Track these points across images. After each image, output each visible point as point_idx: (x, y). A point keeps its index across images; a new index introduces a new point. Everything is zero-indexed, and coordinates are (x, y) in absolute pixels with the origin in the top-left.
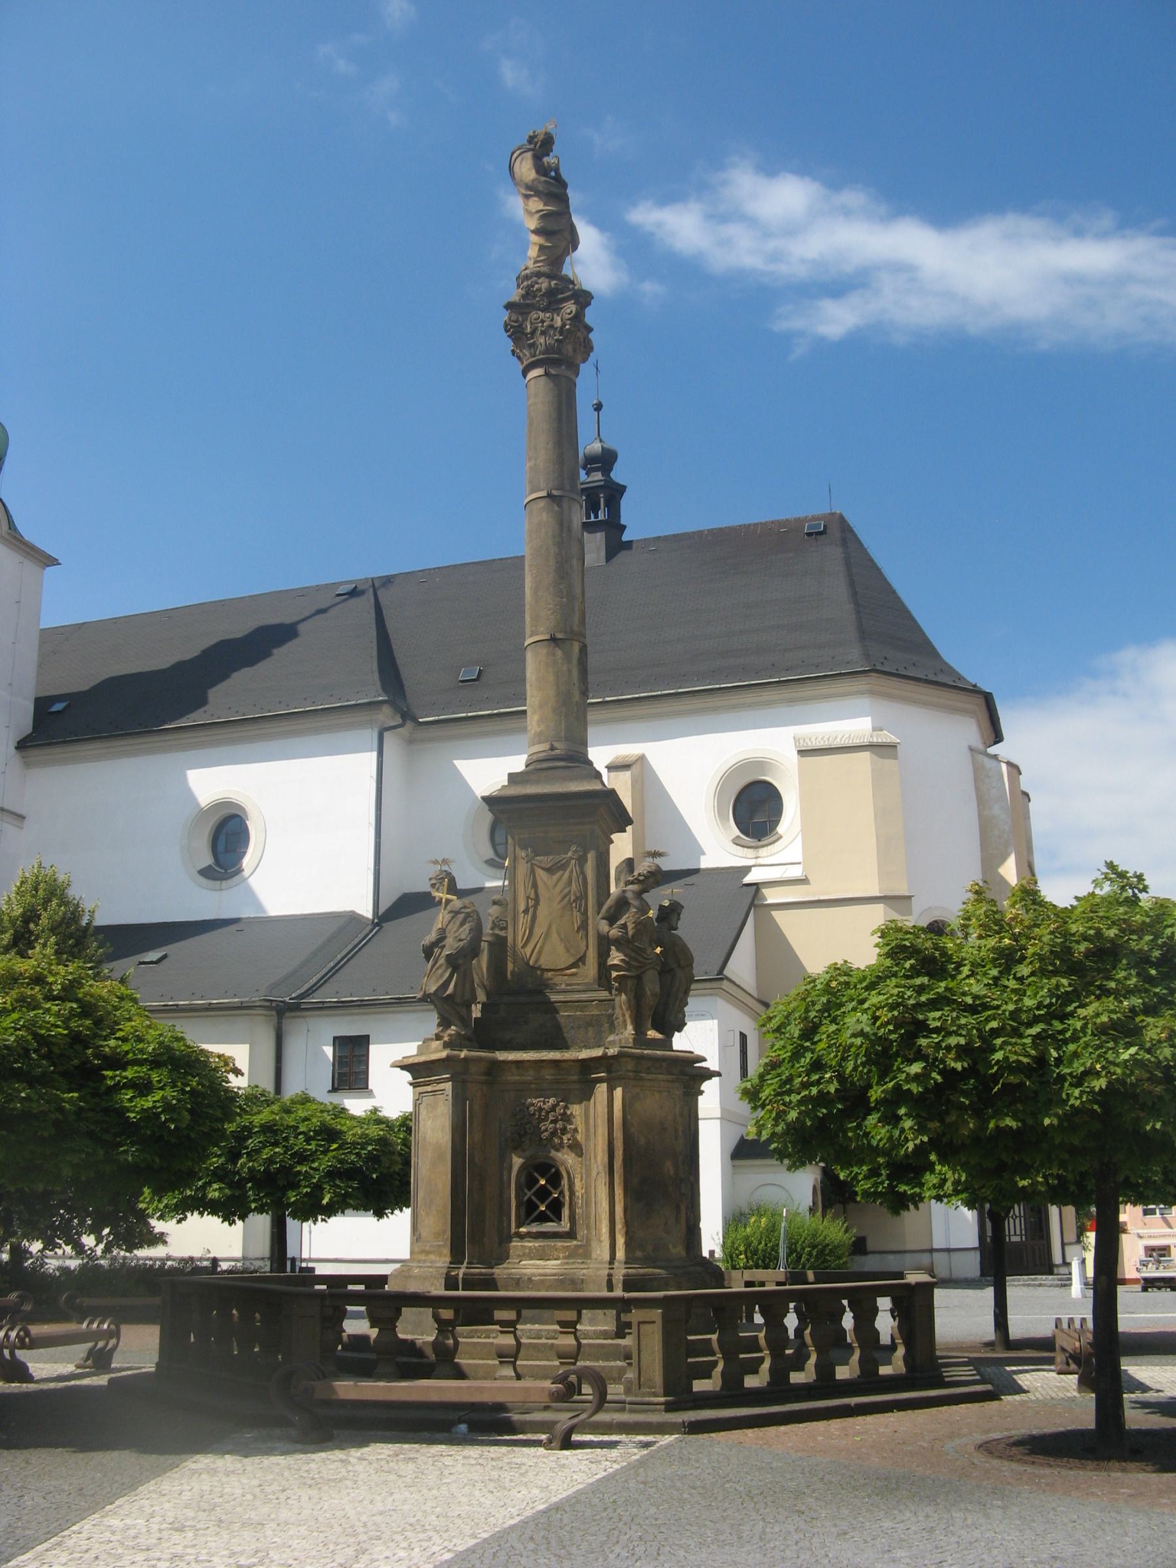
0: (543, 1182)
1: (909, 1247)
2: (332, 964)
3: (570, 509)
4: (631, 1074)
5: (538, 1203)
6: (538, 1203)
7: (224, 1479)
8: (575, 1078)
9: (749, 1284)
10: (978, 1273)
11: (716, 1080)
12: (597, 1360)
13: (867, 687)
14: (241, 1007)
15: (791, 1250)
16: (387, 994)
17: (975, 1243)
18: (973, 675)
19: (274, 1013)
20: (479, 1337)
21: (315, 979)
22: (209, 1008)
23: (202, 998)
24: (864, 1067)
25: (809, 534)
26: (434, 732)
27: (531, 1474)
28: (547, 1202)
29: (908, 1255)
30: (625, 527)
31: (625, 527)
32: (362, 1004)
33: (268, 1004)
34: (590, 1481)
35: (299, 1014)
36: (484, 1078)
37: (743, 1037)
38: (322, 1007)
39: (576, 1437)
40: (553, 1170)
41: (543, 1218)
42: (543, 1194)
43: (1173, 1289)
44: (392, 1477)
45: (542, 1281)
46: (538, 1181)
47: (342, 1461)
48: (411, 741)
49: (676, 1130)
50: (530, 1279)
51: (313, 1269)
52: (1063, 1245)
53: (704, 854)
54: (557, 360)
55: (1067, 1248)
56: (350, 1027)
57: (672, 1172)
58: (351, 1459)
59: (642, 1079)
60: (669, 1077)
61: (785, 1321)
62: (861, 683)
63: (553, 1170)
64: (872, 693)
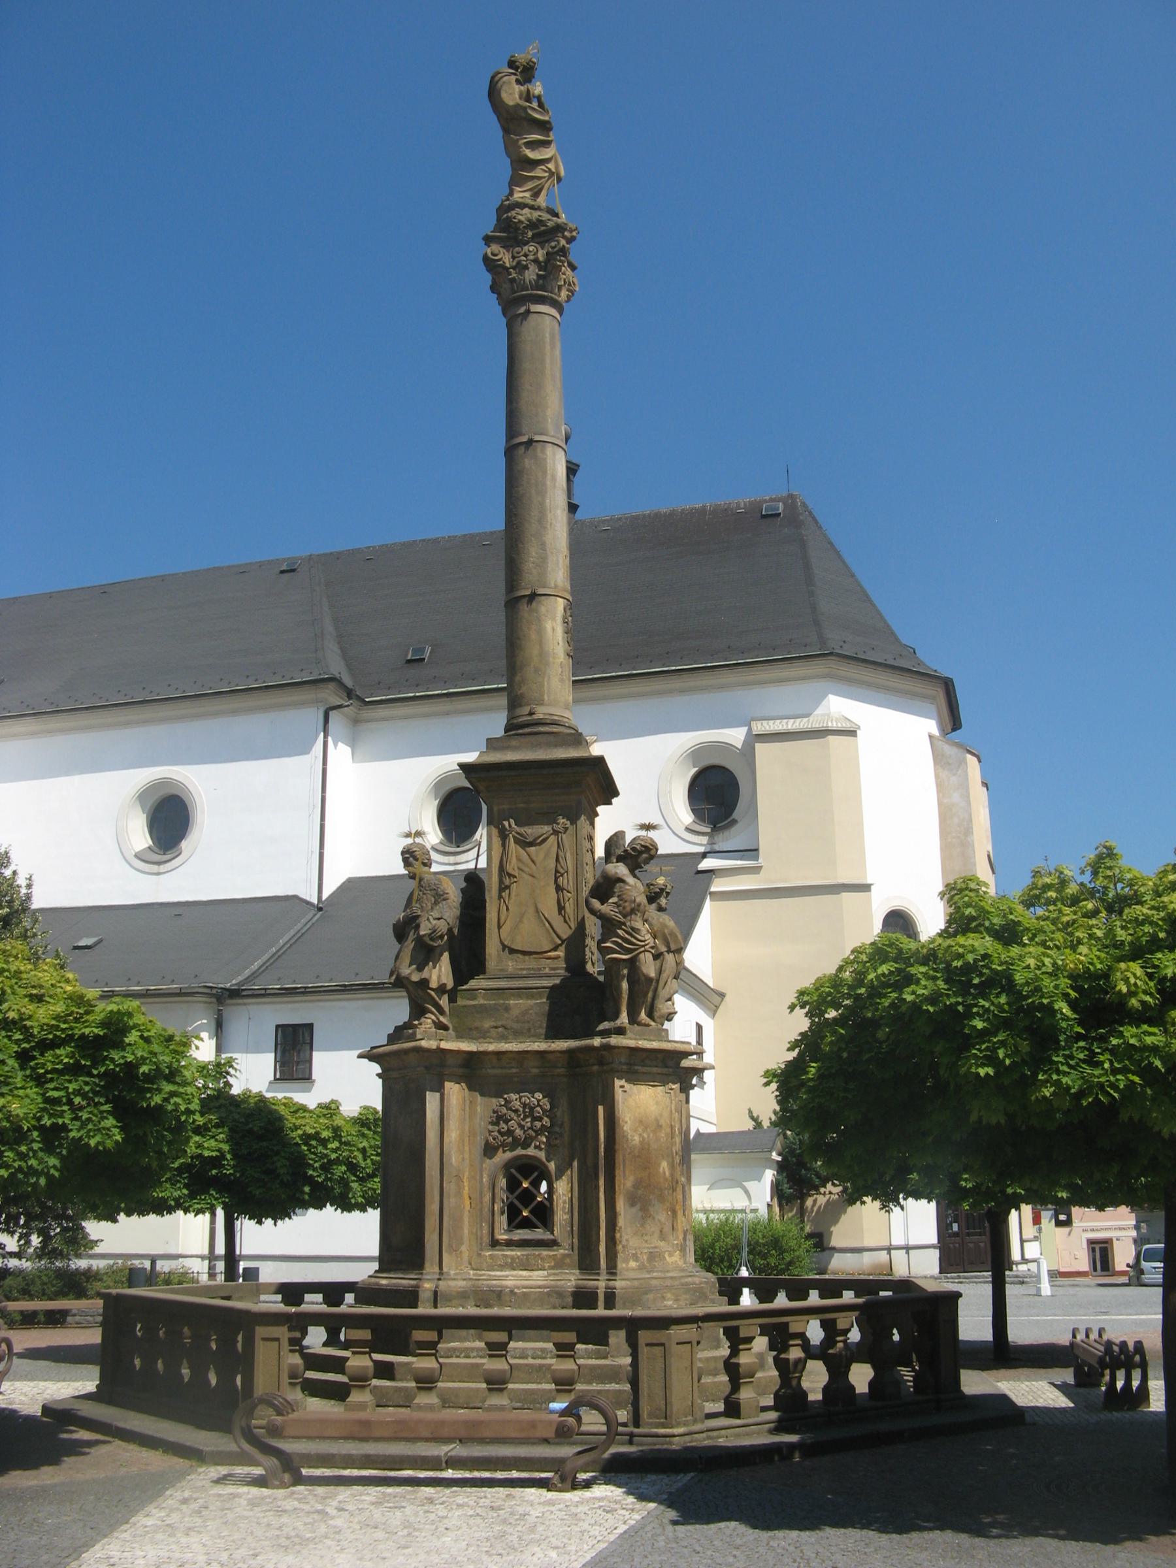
0: (525, 1185)
1: (867, 1243)
2: (274, 950)
3: (554, 454)
4: (625, 1067)
5: (530, 1208)
6: (530, 1208)
7: (184, 1540)
8: (562, 1071)
9: (502, 1213)
10: (937, 1270)
11: (712, 1071)
12: (590, 1383)
14: (180, 994)
15: (749, 1245)
16: (331, 981)
17: (933, 1239)
18: (935, 660)
20: (458, 1357)
21: (256, 965)
23: (138, 984)
24: (1101, 1063)
26: (382, 711)
27: (540, 1528)
29: (866, 1254)
30: (610, 803)
32: (305, 992)
34: (612, 1538)
35: (240, 1001)
37: (699, 1028)
38: (264, 994)
41: (526, 1224)
44: (380, 1534)
45: (525, 1294)
47: (318, 1512)
48: (356, 721)
49: (672, 1127)
50: (512, 1292)
52: (1022, 1241)
55: (1025, 1244)
56: (293, 1013)
57: (667, 1174)
58: (328, 1510)
59: (636, 1072)
60: (665, 1070)
61: (869, 1366)
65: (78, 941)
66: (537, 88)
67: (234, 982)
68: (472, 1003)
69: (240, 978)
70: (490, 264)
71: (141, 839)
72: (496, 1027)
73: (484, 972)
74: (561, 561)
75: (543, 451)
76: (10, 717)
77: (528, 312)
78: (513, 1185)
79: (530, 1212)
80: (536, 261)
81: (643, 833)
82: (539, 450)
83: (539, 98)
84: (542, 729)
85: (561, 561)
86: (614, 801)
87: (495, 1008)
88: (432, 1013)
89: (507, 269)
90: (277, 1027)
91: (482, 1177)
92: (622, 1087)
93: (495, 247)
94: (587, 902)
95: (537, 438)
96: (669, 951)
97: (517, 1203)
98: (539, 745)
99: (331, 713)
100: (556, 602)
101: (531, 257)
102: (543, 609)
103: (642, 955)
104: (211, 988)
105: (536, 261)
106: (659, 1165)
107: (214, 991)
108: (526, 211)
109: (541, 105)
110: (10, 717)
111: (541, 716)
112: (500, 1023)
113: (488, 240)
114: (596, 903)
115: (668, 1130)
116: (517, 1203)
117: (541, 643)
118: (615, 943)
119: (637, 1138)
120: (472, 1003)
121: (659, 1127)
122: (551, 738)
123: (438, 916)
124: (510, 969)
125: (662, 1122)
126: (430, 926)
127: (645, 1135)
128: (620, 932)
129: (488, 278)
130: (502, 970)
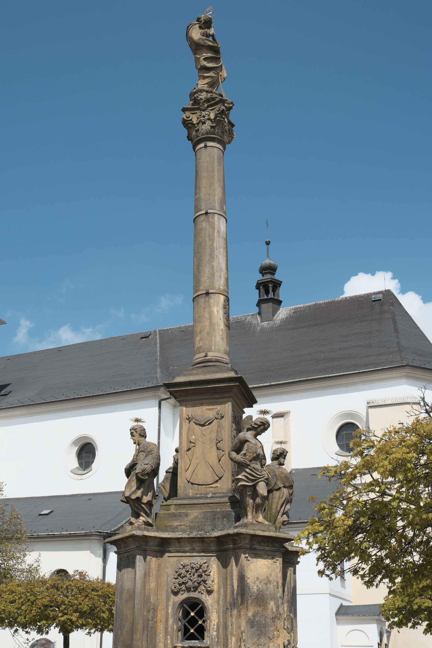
13: (405, 374)
14: (86, 535)
19: (102, 538)
22: (70, 536)
25: (373, 301)
28: (195, 628)
30: (252, 407)
31: (252, 407)
33: (99, 534)
36: (157, 548)
39: (257, 426)
40: (201, 606)
42: (192, 622)
43: (431, 629)
46: (193, 611)
48: (175, 406)
51: (408, 528)
53: (392, 278)
54: (220, 140)
62: (402, 372)
63: (201, 606)
64: (407, 377)
65: (41, 511)
66: (212, 31)
67: (112, 530)
68: (168, 512)
69: (115, 528)
70: (187, 124)
71: (75, 463)
72: (181, 525)
73: (176, 496)
74: (222, 275)
75: (213, 218)
76: (12, 407)
77: (206, 146)
78: (186, 614)
79: (194, 630)
80: (209, 119)
81: (262, 416)
82: (210, 218)
83: (213, 36)
84: (210, 364)
85: (222, 275)
86: (254, 406)
87: (180, 515)
88: (143, 516)
89: (194, 125)
90: (337, 624)
91: (167, 609)
92: (246, 557)
93: (188, 113)
94: (229, 454)
95: (209, 211)
96: (285, 487)
97: (187, 624)
98: (208, 372)
99: (162, 402)
100: (219, 297)
101: (207, 117)
102: (212, 301)
103: (259, 483)
104: (101, 532)
105: (209, 119)
106: (269, 603)
107: (102, 534)
108: (204, 93)
109: (214, 39)
110: (12, 407)
111: (210, 358)
112: (182, 523)
113: (184, 110)
114: (234, 454)
115: (275, 583)
116: (187, 624)
117: (210, 319)
118: (244, 476)
119: (255, 587)
120: (168, 512)
121: (270, 582)
122: (215, 369)
123: (146, 463)
124: (191, 494)
125: (271, 579)
126: (142, 468)
127: (261, 586)
128: (248, 470)
129: (185, 132)
130: (186, 495)
